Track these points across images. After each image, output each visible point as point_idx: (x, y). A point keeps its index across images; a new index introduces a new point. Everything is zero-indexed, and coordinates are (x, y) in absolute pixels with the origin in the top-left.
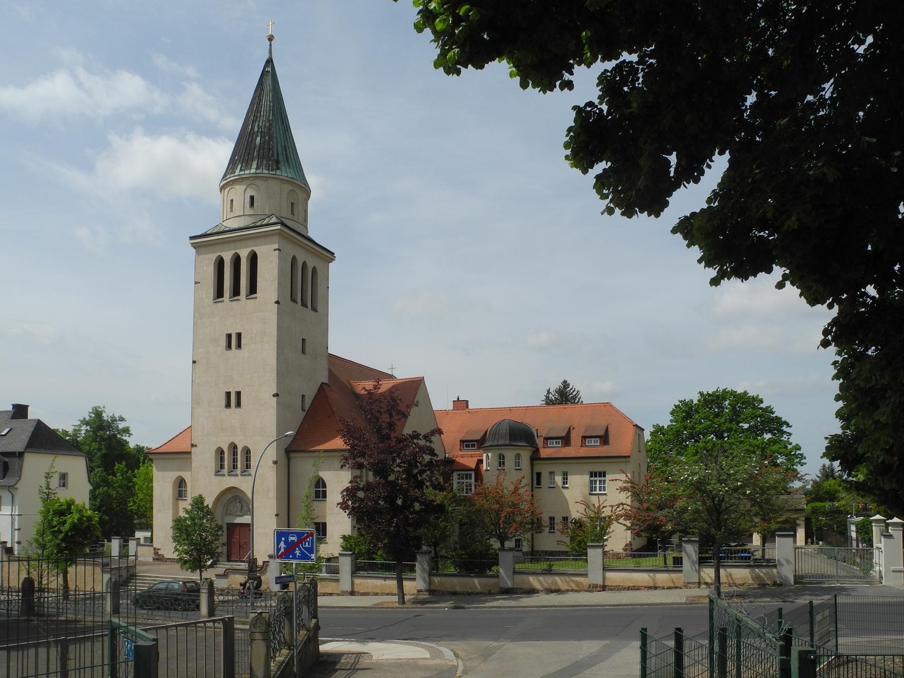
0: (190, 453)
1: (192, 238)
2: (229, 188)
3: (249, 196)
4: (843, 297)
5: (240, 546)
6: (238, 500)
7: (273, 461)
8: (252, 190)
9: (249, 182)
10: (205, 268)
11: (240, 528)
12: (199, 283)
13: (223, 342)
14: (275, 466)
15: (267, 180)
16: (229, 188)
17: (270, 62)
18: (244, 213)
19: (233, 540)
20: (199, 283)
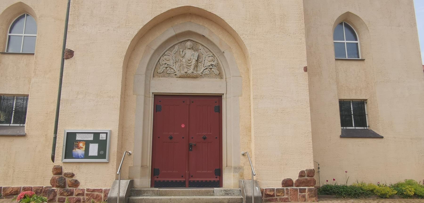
6: (189, 44)
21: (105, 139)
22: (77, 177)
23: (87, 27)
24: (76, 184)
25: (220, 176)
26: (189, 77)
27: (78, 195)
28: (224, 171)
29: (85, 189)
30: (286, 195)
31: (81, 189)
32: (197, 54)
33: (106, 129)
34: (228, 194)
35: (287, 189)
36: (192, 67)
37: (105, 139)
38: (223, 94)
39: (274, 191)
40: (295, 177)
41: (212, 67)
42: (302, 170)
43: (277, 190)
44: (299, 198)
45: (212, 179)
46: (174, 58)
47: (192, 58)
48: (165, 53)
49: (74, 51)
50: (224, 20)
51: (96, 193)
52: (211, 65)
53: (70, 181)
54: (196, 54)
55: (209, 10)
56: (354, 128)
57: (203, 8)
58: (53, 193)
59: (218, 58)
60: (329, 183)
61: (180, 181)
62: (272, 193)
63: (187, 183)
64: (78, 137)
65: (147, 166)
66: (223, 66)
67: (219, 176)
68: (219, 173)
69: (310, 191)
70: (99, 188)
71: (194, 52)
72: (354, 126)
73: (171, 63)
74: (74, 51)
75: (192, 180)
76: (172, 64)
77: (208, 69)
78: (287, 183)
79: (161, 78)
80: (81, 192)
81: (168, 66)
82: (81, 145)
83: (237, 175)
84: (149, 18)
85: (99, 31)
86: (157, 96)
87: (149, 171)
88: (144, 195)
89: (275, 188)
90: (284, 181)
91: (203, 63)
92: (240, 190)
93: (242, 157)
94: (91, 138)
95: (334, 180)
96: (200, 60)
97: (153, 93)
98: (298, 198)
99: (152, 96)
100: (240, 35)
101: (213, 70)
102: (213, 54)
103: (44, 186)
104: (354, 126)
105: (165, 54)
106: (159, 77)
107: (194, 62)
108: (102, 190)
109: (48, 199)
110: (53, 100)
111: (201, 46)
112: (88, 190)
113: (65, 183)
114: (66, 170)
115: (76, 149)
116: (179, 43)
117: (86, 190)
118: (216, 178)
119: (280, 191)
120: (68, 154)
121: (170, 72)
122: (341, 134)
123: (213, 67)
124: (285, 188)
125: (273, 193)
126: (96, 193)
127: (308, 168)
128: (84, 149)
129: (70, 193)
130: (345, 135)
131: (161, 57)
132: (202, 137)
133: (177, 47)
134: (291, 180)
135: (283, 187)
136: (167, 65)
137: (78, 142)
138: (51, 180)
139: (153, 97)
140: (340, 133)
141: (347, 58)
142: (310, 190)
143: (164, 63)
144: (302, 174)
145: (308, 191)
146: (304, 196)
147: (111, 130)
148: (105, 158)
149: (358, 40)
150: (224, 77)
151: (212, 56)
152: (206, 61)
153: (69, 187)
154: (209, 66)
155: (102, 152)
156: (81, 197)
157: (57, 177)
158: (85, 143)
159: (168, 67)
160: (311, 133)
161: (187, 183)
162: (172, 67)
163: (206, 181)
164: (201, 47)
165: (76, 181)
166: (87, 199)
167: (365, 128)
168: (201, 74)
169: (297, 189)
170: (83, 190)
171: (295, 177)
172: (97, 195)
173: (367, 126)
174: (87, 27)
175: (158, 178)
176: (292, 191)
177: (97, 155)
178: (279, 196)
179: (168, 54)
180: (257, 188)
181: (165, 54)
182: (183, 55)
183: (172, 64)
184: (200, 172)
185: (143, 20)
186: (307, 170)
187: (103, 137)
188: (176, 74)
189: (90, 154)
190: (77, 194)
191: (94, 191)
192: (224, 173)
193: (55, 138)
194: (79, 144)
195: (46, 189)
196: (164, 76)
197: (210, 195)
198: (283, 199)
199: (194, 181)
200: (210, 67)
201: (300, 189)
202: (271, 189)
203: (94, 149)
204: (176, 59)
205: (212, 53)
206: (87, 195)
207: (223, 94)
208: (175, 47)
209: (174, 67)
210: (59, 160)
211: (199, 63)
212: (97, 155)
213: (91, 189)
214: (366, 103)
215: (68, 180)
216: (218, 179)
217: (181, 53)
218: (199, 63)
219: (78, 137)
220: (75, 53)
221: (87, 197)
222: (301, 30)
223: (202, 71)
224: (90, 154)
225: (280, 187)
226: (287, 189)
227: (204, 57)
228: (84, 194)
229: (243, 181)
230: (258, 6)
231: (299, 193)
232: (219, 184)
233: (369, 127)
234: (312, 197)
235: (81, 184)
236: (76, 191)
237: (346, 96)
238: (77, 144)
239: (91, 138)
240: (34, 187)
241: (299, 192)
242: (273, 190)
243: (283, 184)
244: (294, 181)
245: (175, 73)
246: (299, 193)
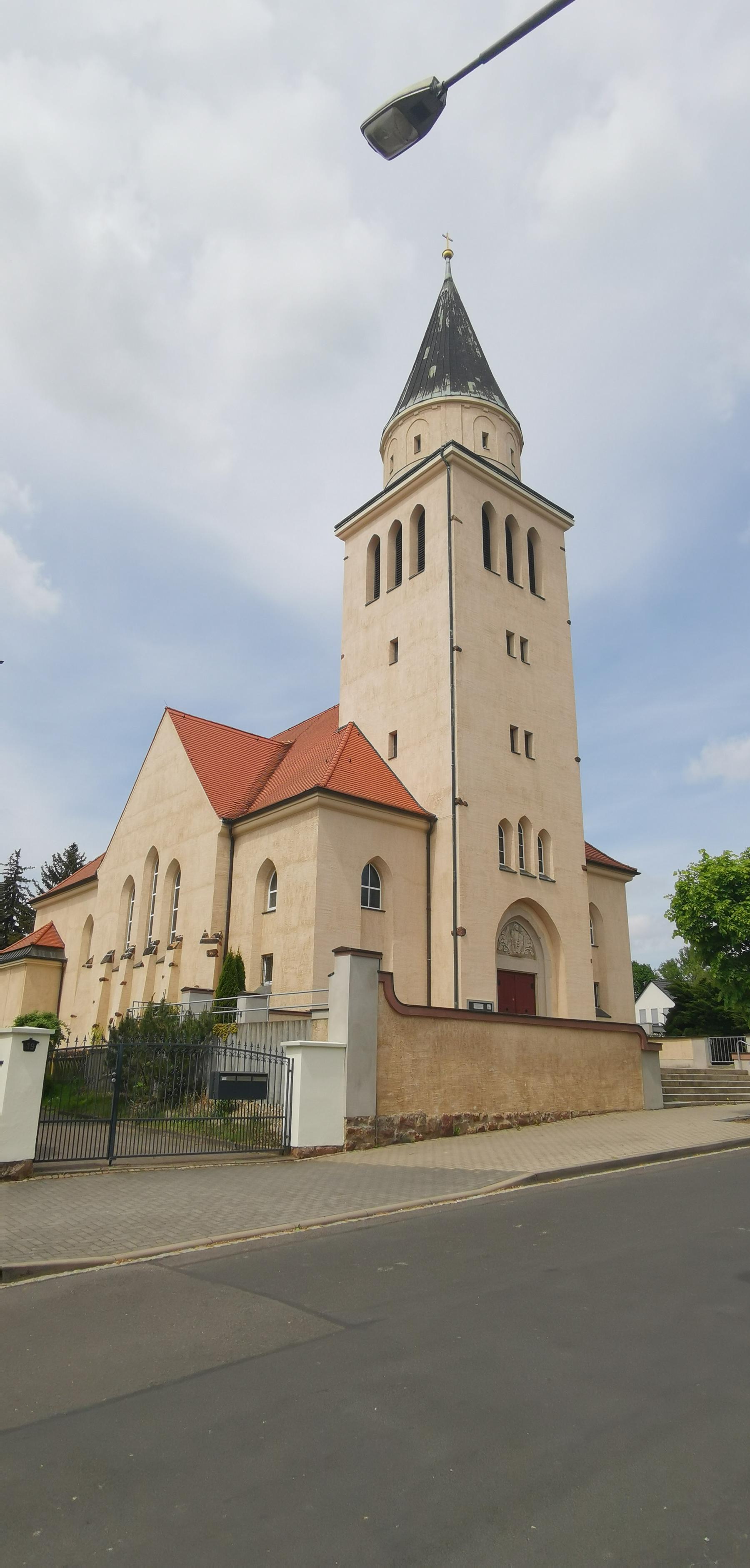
1: (338, 527)
17: (449, 281)
141: (369, 907)
149: (381, 887)
173: (133, 947)
188: (509, 953)
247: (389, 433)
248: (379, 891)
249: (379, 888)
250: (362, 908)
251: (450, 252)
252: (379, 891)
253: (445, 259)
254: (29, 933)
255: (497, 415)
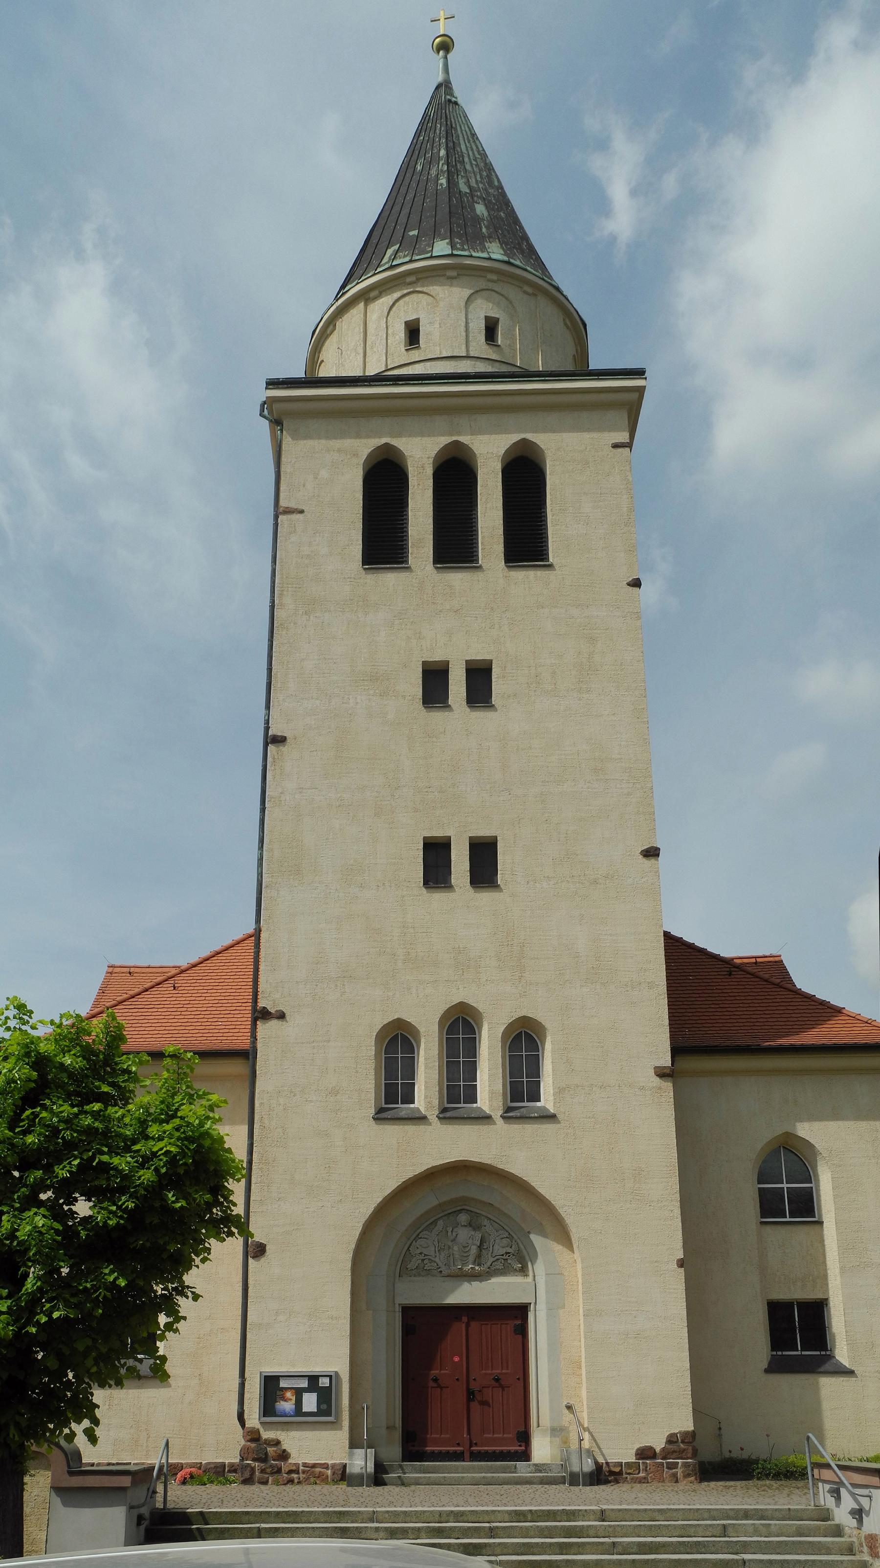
0: (248, 1055)
2: (396, 295)
3: (482, 316)
4: (141, 1160)
5: (471, 1395)
6: (463, 1218)
7: (656, 1068)
8: (491, 305)
9: (482, 284)
10: (324, 474)
11: (468, 1325)
12: (302, 512)
13: (414, 685)
14: (668, 1086)
15: (534, 295)
16: (396, 295)
17: (445, 86)
18: (468, 351)
19: (434, 1372)
20: (302, 512)
21: (328, 1385)
22: (285, 1446)
23: (285, 1203)
24: (284, 1456)
25: (522, 1335)
26: (465, 1276)
27: (290, 1472)
28: (533, 1434)
29: (300, 1462)
30: (643, 1473)
31: (294, 1464)
32: (480, 1235)
33: (331, 1369)
34: (540, 1471)
35: (645, 1464)
36: (471, 1258)
37: (328, 1385)
38: (530, 1303)
39: (622, 1466)
40: (659, 1444)
41: (507, 1257)
42: (672, 1432)
43: (627, 1464)
44: (666, 1477)
45: (513, 1448)
46: (436, 1243)
47: (470, 1241)
48: (418, 1235)
49: (266, 1245)
50: (529, 1182)
51: (318, 1470)
52: (507, 1253)
53: (275, 1452)
54: (478, 1235)
55: (501, 1166)
56: (799, 1353)
57: (489, 1162)
58: (249, 1469)
59: (518, 1240)
60: (734, 1455)
61: (455, 1452)
62: (617, 1470)
63: (467, 1455)
64: (283, 1384)
65: (395, 1427)
66: (528, 1254)
67: (521, 1336)
68: (525, 1438)
69: (685, 1466)
70: (323, 1462)
71: (473, 1233)
72: (800, 1349)
73: (431, 1251)
74: (266, 1245)
75: (475, 1450)
76: (432, 1253)
77: (500, 1261)
78: (645, 1453)
79: (413, 1278)
80: (294, 1468)
81: (426, 1257)
82: (289, 1394)
83: (557, 1440)
84: (392, 1185)
85: (306, 1210)
86: (406, 1310)
87: (398, 1435)
88: (398, 1472)
89: (624, 1461)
90: (638, 1450)
91: (491, 1251)
92: (562, 1465)
93: (566, 1411)
94: (304, 1384)
95: (742, 1449)
96: (484, 1244)
97: (399, 1304)
98: (664, 1476)
99: (398, 1309)
100: (559, 1208)
101: (509, 1261)
102: (509, 1234)
103: (204, 1462)
104: (800, 1349)
105: (420, 1237)
106: (410, 1276)
107: (474, 1250)
108: (328, 1464)
109: (242, 1479)
110: (209, 1315)
111: (486, 1220)
112: (305, 1465)
113: (266, 1454)
114: (266, 1435)
115: (281, 1402)
116: (445, 1215)
117: (301, 1465)
118: (520, 1446)
119: (632, 1466)
120: (268, 1408)
121: (430, 1268)
122: (768, 1367)
123: (509, 1256)
124: (641, 1461)
125: (620, 1468)
126: (318, 1470)
127: (683, 1430)
128: (294, 1401)
129: (276, 1469)
130: (777, 1366)
131: (412, 1242)
132: (492, 1378)
133: (440, 1223)
134: (651, 1449)
135: (636, 1459)
136: (423, 1255)
137: (283, 1391)
138: (241, 1451)
139: (401, 1310)
140: (765, 1365)
141: (788, 1219)
142: (685, 1465)
143: (418, 1251)
144: (671, 1440)
145: (682, 1465)
146: (675, 1475)
147: (336, 1373)
148: (330, 1415)
149: (813, 1182)
150: (531, 1273)
151: (507, 1238)
152: (496, 1247)
153: (274, 1460)
154: (503, 1255)
155: (324, 1407)
156: (295, 1476)
157: (253, 1445)
158: (294, 1391)
159: (425, 1259)
160: (689, 1372)
161: (467, 1455)
162: (433, 1259)
163: (502, 1452)
164: (486, 1222)
165: (284, 1451)
166: (305, 1478)
167: (823, 1353)
168: (488, 1270)
169: (663, 1463)
170: (297, 1465)
171: (659, 1444)
172: (320, 1472)
173: (829, 1349)
174: (285, 1203)
175: (414, 1446)
176: (653, 1466)
177: (316, 1411)
178: (629, 1474)
179: (425, 1236)
180: (589, 1460)
181: (420, 1237)
182: (452, 1238)
183: (432, 1253)
184: (489, 1436)
185: (383, 1188)
186: (680, 1432)
187: (324, 1382)
188: (441, 1272)
189: (305, 1409)
190: (287, 1470)
191: (314, 1466)
192: (533, 1438)
193: (242, 1385)
194: (284, 1394)
195: (209, 1467)
196: (420, 1275)
197: (511, 1472)
198: (637, 1478)
199: (479, 1452)
200: (504, 1257)
201: (667, 1463)
202: (616, 1462)
203: (310, 1402)
204: (440, 1243)
205: (507, 1231)
206: (304, 1472)
207: (530, 1303)
208: (438, 1224)
209: (437, 1260)
210: (253, 1419)
211: (483, 1251)
212: (316, 1411)
213: (309, 1464)
214: (827, 1305)
215: (270, 1450)
216: (523, 1448)
217: (450, 1234)
218: (483, 1251)
219: (283, 1384)
220: (267, 1248)
221: (304, 1476)
222: (673, 1195)
223: (489, 1264)
224: (305, 1409)
225: (633, 1459)
226: (645, 1464)
227: (493, 1240)
228: (299, 1471)
229: (567, 1451)
230: (592, 1155)
231: (666, 1470)
232: (525, 1456)
233: (831, 1350)
234: (689, 1475)
235: (292, 1456)
236: (285, 1467)
237: (782, 1294)
238: (282, 1393)
239: (304, 1384)
240: (185, 1463)
241: (667, 1468)
242: (620, 1464)
243: (636, 1454)
244: (658, 1450)
245: (439, 1270)
246: (666, 1470)
247: (315, 355)
248: (812, 1188)
249: (811, 1183)
250: (762, 1223)
251: (452, 44)
252: (812, 1188)
253: (438, 53)
254: (10, 1299)
255: (482, 277)
